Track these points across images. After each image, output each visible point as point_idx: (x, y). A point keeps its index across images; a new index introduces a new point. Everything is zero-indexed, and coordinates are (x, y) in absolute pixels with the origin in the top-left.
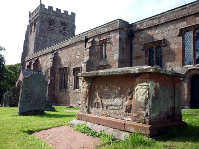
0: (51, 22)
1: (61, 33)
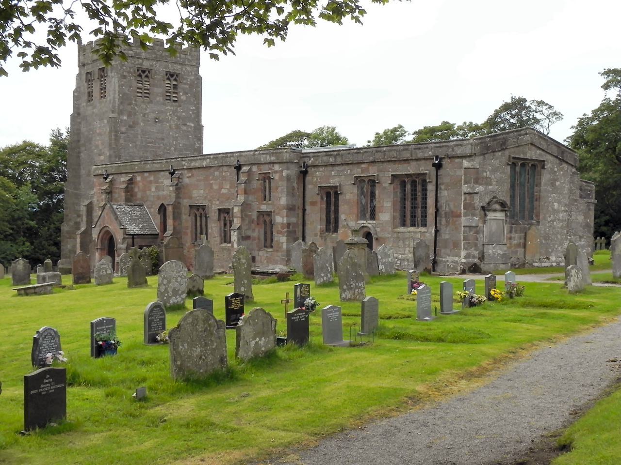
1: (167, 100)
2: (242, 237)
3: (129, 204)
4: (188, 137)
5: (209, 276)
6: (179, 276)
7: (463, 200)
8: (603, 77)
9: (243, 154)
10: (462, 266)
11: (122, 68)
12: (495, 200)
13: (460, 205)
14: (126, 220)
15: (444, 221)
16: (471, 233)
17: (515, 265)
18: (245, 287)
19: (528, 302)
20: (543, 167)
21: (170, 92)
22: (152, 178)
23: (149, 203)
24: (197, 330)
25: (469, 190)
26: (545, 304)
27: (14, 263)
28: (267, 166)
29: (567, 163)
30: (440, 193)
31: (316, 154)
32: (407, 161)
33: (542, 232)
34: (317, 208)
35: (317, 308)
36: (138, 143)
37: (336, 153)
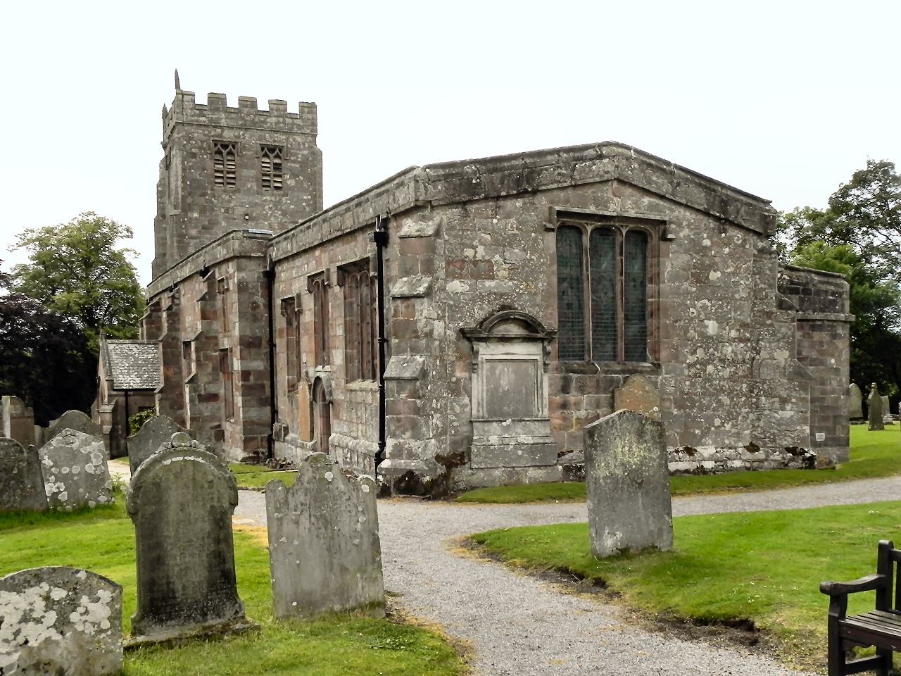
0: (224, 149)
1: (264, 186)
2: (200, 395)
11: (188, 142)
16: (403, 396)
21: (269, 175)
29: (740, 227)
33: (670, 389)
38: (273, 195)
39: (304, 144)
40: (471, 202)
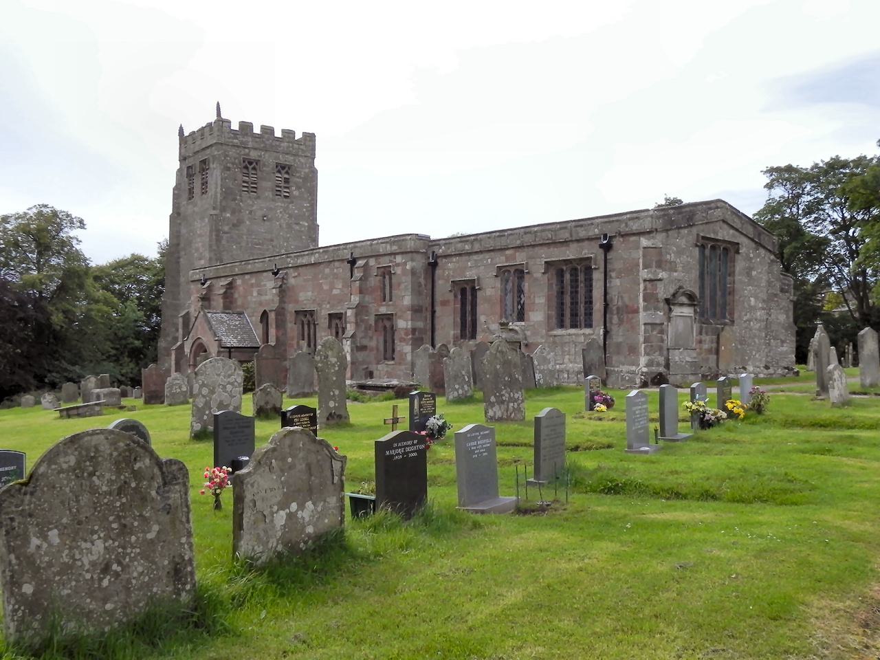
0: (250, 165)
1: (277, 195)
2: (357, 347)
3: (227, 311)
4: (301, 237)
5: (308, 393)
6: (229, 383)
7: (641, 290)
8: (765, 175)
9: (358, 245)
10: (642, 377)
11: (225, 158)
12: (681, 290)
13: (637, 296)
14: (221, 330)
15: (615, 319)
16: (655, 333)
17: (707, 376)
18: (335, 401)
19: (790, 419)
20: (737, 252)
21: (280, 187)
22: (253, 281)
23: (249, 310)
24: (94, 490)
25: (650, 276)
26: (822, 423)
27: (84, 381)
28: (387, 258)
29: (764, 247)
30: (610, 282)
31: (447, 241)
32: (565, 243)
34: (450, 309)
35: (448, 432)
36: (243, 244)
37: (472, 238)
38: (283, 202)
39: (306, 164)
40: (670, 230)
